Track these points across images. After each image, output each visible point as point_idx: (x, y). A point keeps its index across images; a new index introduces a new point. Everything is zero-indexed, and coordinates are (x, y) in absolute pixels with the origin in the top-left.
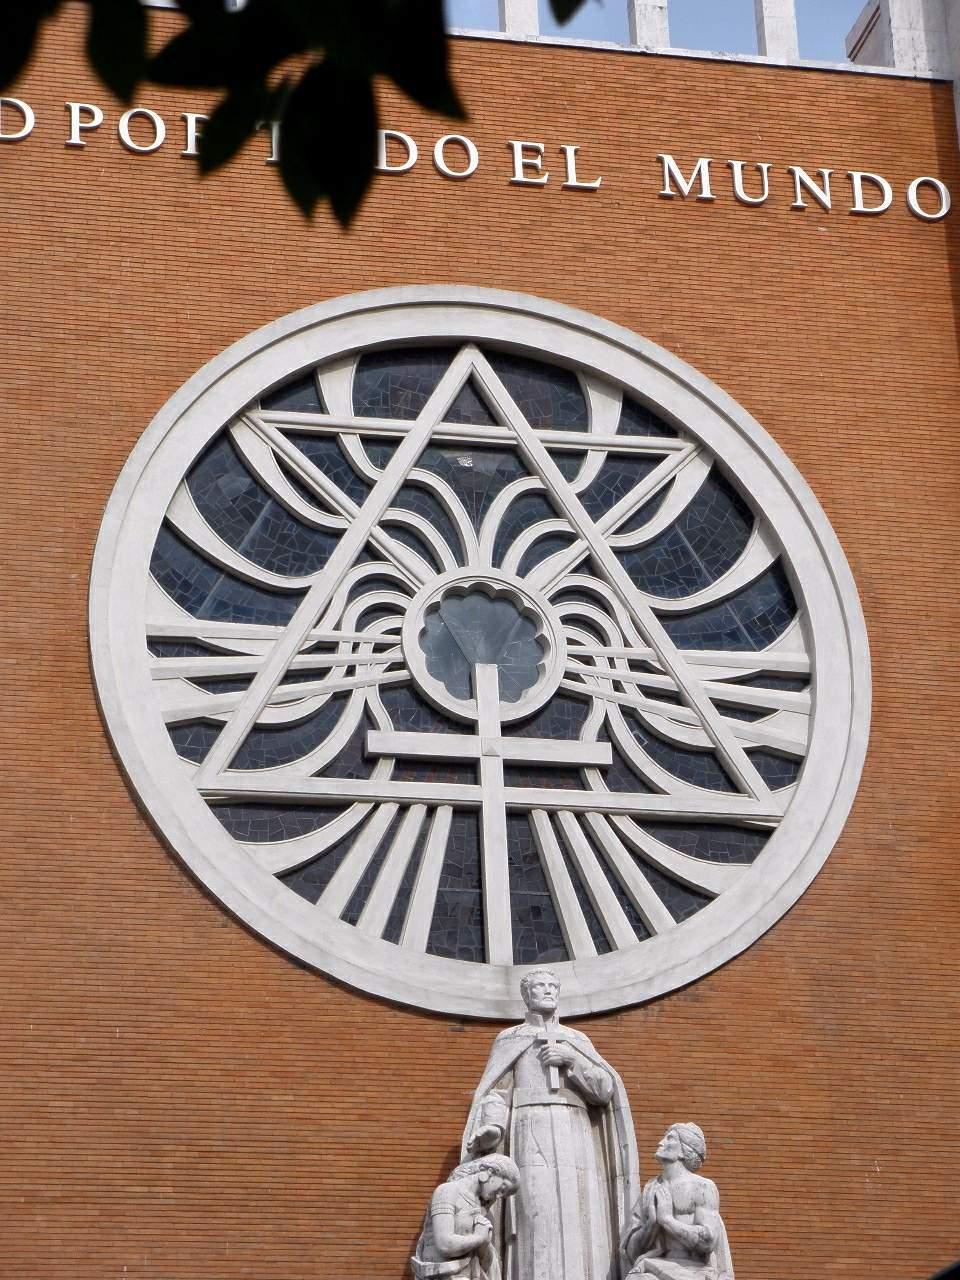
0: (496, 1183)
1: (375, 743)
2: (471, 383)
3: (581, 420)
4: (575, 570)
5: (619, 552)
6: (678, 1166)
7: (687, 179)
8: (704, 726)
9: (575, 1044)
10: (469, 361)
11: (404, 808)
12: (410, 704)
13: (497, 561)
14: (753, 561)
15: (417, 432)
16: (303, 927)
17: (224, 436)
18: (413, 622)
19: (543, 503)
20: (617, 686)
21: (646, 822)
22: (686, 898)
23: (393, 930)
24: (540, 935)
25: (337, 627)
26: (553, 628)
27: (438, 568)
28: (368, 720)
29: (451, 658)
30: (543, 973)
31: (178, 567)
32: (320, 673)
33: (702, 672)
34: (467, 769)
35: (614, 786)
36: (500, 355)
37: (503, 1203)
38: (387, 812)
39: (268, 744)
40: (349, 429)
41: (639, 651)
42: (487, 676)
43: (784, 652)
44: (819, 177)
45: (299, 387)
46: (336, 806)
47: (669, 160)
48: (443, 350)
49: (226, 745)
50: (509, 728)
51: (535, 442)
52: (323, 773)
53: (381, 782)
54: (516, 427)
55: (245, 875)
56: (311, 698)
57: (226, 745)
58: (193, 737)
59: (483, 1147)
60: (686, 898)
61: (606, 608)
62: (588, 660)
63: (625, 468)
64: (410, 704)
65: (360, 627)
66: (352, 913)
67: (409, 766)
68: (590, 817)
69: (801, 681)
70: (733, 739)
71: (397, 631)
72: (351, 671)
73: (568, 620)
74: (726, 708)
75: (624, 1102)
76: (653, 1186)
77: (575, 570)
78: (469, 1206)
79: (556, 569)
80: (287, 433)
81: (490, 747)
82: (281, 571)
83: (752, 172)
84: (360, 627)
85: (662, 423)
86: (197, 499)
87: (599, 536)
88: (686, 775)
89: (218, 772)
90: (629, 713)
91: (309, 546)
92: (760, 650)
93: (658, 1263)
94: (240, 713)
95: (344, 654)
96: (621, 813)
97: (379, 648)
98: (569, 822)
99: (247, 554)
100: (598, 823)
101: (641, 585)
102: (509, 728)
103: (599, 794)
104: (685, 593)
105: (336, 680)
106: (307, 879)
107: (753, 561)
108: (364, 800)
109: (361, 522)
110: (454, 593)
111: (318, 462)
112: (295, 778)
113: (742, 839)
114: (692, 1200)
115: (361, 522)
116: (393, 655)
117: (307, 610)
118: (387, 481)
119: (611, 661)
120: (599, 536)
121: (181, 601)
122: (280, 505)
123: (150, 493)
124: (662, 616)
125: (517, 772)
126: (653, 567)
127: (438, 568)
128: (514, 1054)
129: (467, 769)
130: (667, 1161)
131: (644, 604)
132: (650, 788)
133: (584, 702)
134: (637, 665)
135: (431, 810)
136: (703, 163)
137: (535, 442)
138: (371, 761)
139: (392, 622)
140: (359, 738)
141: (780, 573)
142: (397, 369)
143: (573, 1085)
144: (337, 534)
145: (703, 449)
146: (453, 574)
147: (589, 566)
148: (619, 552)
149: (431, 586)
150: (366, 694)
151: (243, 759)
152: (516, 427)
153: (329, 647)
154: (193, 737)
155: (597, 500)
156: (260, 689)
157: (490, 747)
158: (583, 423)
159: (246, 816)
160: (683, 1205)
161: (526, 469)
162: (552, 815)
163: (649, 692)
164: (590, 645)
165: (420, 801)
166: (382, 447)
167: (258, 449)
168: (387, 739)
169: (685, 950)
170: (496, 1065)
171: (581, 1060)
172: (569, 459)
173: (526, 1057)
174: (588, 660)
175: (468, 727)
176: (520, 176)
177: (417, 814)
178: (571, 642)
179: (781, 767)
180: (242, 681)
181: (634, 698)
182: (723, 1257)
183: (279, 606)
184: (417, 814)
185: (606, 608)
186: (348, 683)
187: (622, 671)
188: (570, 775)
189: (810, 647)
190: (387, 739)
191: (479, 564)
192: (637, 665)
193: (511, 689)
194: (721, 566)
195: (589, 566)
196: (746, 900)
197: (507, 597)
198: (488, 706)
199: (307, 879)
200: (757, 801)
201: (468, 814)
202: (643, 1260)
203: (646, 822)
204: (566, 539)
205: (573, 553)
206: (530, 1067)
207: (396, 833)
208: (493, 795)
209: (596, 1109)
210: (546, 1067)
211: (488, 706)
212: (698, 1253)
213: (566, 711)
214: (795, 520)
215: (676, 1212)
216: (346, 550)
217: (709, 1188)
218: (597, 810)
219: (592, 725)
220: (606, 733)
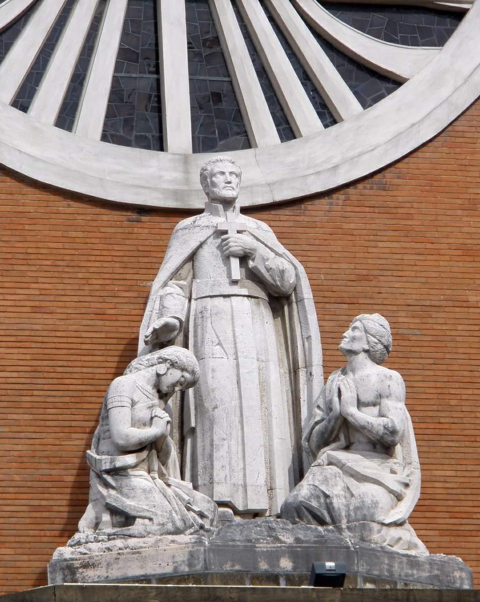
0: (175, 375)
6: (362, 356)
9: (257, 235)
22: (374, 83)
23: (67, 117)
37: (182, 397)
59: (161, 339)
60: (374, 83)
75: (307, 292)
76: (337, 378)
78: (147, 400)
93: (342, 456)
110: (209, 392)
114: (377, 391)
130: (352, 352)
143: (254, 276)
160: (367, 397)
169: (373, 137)
170: (175, 256)
171: (262, 250)
182: (408, 449)
202: (327, 453)
206: (209, 257)
209: (278, 300)
210: (227, 258)
212: (383, 446)
217: (395, 381)
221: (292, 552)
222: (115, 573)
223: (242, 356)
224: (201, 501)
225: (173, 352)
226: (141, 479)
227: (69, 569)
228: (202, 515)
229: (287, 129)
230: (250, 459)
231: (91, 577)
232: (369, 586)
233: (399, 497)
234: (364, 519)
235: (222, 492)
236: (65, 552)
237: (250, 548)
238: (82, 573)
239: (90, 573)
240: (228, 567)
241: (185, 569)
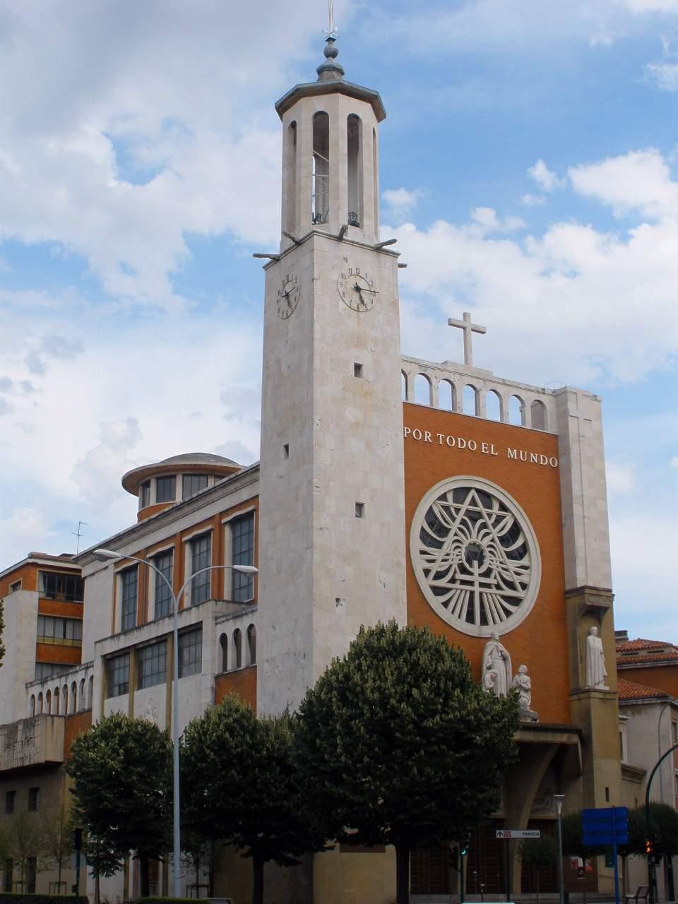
2: (473, 498)
3: (490, 507)
8: (512, 576)
10: (473, 493)
11: (462, 590)
12: (464, 570)
14: (519, 542)
16: (445, 614)
17: (431, 507)
18: (463, 551)
20: (497, 567)
22: (508, 613)
24: (484, 621)
26: (487, 553)
28: (455, 572)
29: (469, 561)
30: (484, 627)
31: (424, 536)
33: (512, 564)
34: (471, 583)
35: (497, 589)
36: (478, 491)
38: (459, 591)
39: (439, 575)
40: (452, 506)
41: (501, 560)
42: (476, 563)
43: (524, 562)
44: (535, 456)
46: (448, 590)
48: (469, 489)
49: (432, 575)
50: (480, 575)
51: (484, 511)
53: (457, 585)
54: (481, 508)
59: (489, 668)
62: (492, 561)
63: (499, 519)
67: (463, 582)
70: (517, 580)
72: (452, 560)
73: (490, 552)
79: (486, 541)
80: (442, 506)
82: (439, 536)
83: (524, 454)
90: (499, 573)
94: (435, 568)
97: (457, 555)
98: (489, 596)
100: (494, 596)
101: (502, 545)
102: (480, 575)
103: (494, 590)
105: (450, 562)
106: (446, 604)
107: (519, 542)
108: (455, 589)
109: (454, 527)
112: (442, 583)
113: (516, 601)
116: (459, 557)
117: (445, 546)
123: (420, 521)
125: (482, 585)
127: (467, 538)
129: (471, 583)
131: (503, 549)
134: (501, 563)
135: (466, 591)
136: (515, 450)
137: (484, 511)
139: (459, 550)
142: (460, 493)
144: (450, 529)
145: (513, 515)
146: (470, 540)
148: (498, 537)
150: (455, 567)
152: (481, 508)
157: (477, 579)
159: (438, 591)
161: (482, 517)
162: (486, 594)
164: (493, 558)
166: (458, 510)
168: (460, 576)
172: (490, 515)
174: (492, 561)
175: (471, 574)
177: (464, 592)
179: (524, 586)
180: (433, 561)
183: (439, 545)
184: (464, 592)
186: (452, 563)
187: (498, 563)
188: (488, 586)
189: (530, 561)
191: (474, 539)
192: (501, 563)
195: (493, 540)
196: (520, 614)
198: (476, 569)
201: (472, 593)
203: (503, 597)
204: (487, 534)
205: (489, 537)
207: (459, 594)
208: (477, 589)
209: (504, 659)
213: (487, 573)
214: (529, 534)
216: (451, 534)
219: (493, 575)
220: (495, 578)
225: (493, 670)
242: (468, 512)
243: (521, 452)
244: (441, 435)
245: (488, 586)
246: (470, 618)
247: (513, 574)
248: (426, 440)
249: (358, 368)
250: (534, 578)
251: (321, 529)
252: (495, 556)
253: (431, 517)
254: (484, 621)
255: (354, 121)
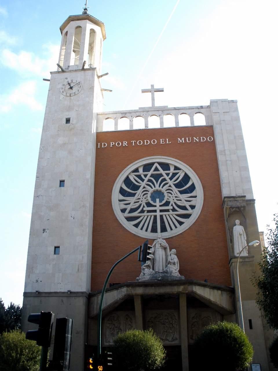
1: (144, 209)
4: (168, 187)
5: (174, 184)
7: (181, 140)
8: (183, 203)
10: (156, 165)
12: (149, 204)
13: (159, 187)
15: (150, 173)
18: (149, 195)
19: (164, 180)
20: (173, 200)
21: (177, 215)
22: (181, 223)
23: (146, 230)
25: (140, 196)
26: (166, 194)
27: (152, 188)
28: (144, 207)
29: (153, 198)
31: (122, 192)
32: (138, 202)
36: (160, 164)
38: (149, 217)
39: (132, 211)
40: (142, 174)
41: (176, 195)
42: (158, 200)
45: (136, 170)
47: (179, 139)
49: (127, 211)
50: (160, 206)
52: (139, 213)
53: (145, 214)
54: (161, 171)
55: (129, 226)
56: (137, 205)
57: (127, 211)
58: (123, 211)
60: (181, 223)
61: (172, 191)
62: (170, 197)
64: (149, 204)
65: (143, 196)
66: (171, 229)
67: (149, 211)
68: (170, 215)
69: (195, 197)
70: (187, 205)
71: (147, 196)
72: (142, 201)
73: (167, 193)
74: (186, 201)
75: (168, 247)
77: (168, 187)
79: (166, 187)
81: (158, 208)
82: (134, 191)
83: (189, 140)
84: (143, 196)
85: (179, 169)
86: (125, 184)
87: (171, 183)
88: (182, 209)
89: (126, 214)
90: (175, 203)
91: (137, 188)
92: (191, 193)
94: (129, 207)
95: (141, 200)
96: (173, 214)
97: (145, 198)
99: (130, 189)
102: (160, 206)
103: (171, 212)
104: (182, 188)
105: (140, 202)
106: (136, 226)
108: (143, 216)
109: (143, 184)
111: (139, 178)
113: (187, 216)
115: (143, 184)
116: (147, 199)
118: (146, 179)
119: (173, 197)
120: (171, 183)
121: (123, 195)
122: (134, 184)
123: (119, 183)
124: (179, 191)
125: (161, 211)
126: (177, 186)
127: (152, 188)
128: (155, 243)
129: (155, 211)
132: (177, 211)
133: (169, 202)
135: (151, 216)
136: (183, 139)
138: (144, 211)
140: (143, 209)
141: (193, 185)
142: (147, 167)
147: (170, 186)
149: (151, 190)
150: (144, 204)
151: (130, 212)
153: (139, 199)
154: (123, 211)
155: (171, 179)
156: (131, 204)
157: (158, 208)
158: (169, 170)
159: (129, 219)
161: (163, 176)
162: (165, 215)
163: (177, 200)
164: (170, 195)
165: (146, 215)
166: (146, 176)
167: (132, 178)
168: (146, 209)
172: (168, 174)
173: (157, 244)
174: (170, 197)
175: (156, 206)
176: (161, 143)
178: (168, 195)
179: (193, 207)
180: (129, 204)
181: (175, 201)
183: (133, 195)
184: (149, 217)
185: (172, 191)
187: (174, 198)
188: (168, 211)
190: (146, 209)
192: (176, 197)
193: (160, 201)
194: (186, 185)
196: (188, 223)
197: (160, 191)
199: (136, 226)
200: (190, 211)
201: (155, 217)
203: (177, 215)
204: (167, 184)
208: (158, 214)
209: (165, 249)
211: (158, 203)
213: (167, 204)
214: (195, 179)
215: (172, 260)
218: (171, 214)
220: (172, 205)
221: (161, 277)
222: (142, 280)
223: (160, 254)
224: (154, 272)
226: (146, 270)
227: (138, 280)
228: (153, 273)
229: (171, 229)
230: (160, 266)
231: (140, 281)
232: (170, 280)
233: (176, 270)
234: (171, 272)
235: (157, 270)
236: (138, 278)
237: (156, 277)
238: (139, 280)
239: (141, 280)
240: (154, 279)
241: (149, 279)
242: (152, 176)
243: (187, 138)
244: (133, 141)
245: (168, 211)
246: (154, 230)
247: (185, 202)
248: (124, 145)
249: (68, 121)
250: (199, 202)
251: (37, 197)
252: (172, 195)
253: (127, 181)
254: (164, 229)
255: (93, 31)
